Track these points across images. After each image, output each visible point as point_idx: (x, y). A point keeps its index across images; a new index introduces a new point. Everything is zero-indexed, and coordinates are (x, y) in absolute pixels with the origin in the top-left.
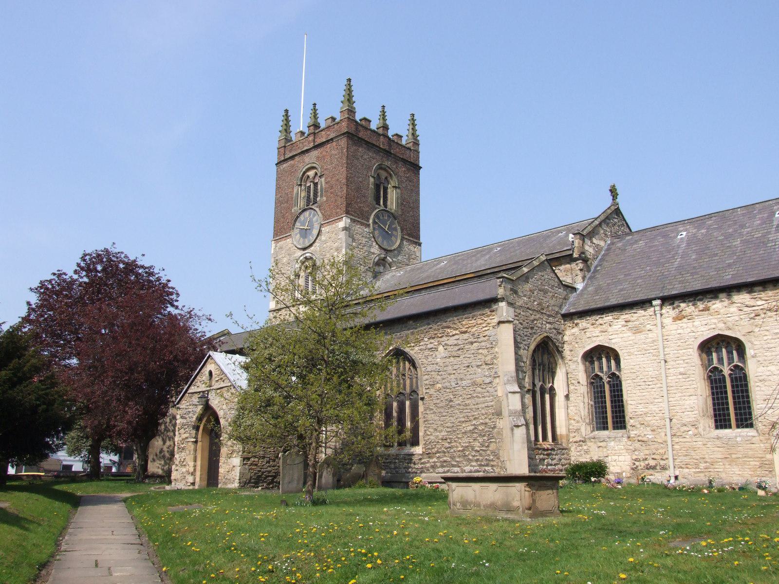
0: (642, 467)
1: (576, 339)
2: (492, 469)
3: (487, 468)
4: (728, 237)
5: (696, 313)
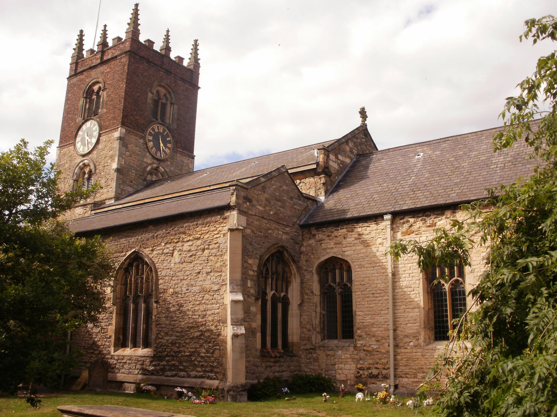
0: (366, 376)
1: (312, 250)
2: (215, 375)
3: (210, 374)
4: (457, 158)
5: (423, 229)
